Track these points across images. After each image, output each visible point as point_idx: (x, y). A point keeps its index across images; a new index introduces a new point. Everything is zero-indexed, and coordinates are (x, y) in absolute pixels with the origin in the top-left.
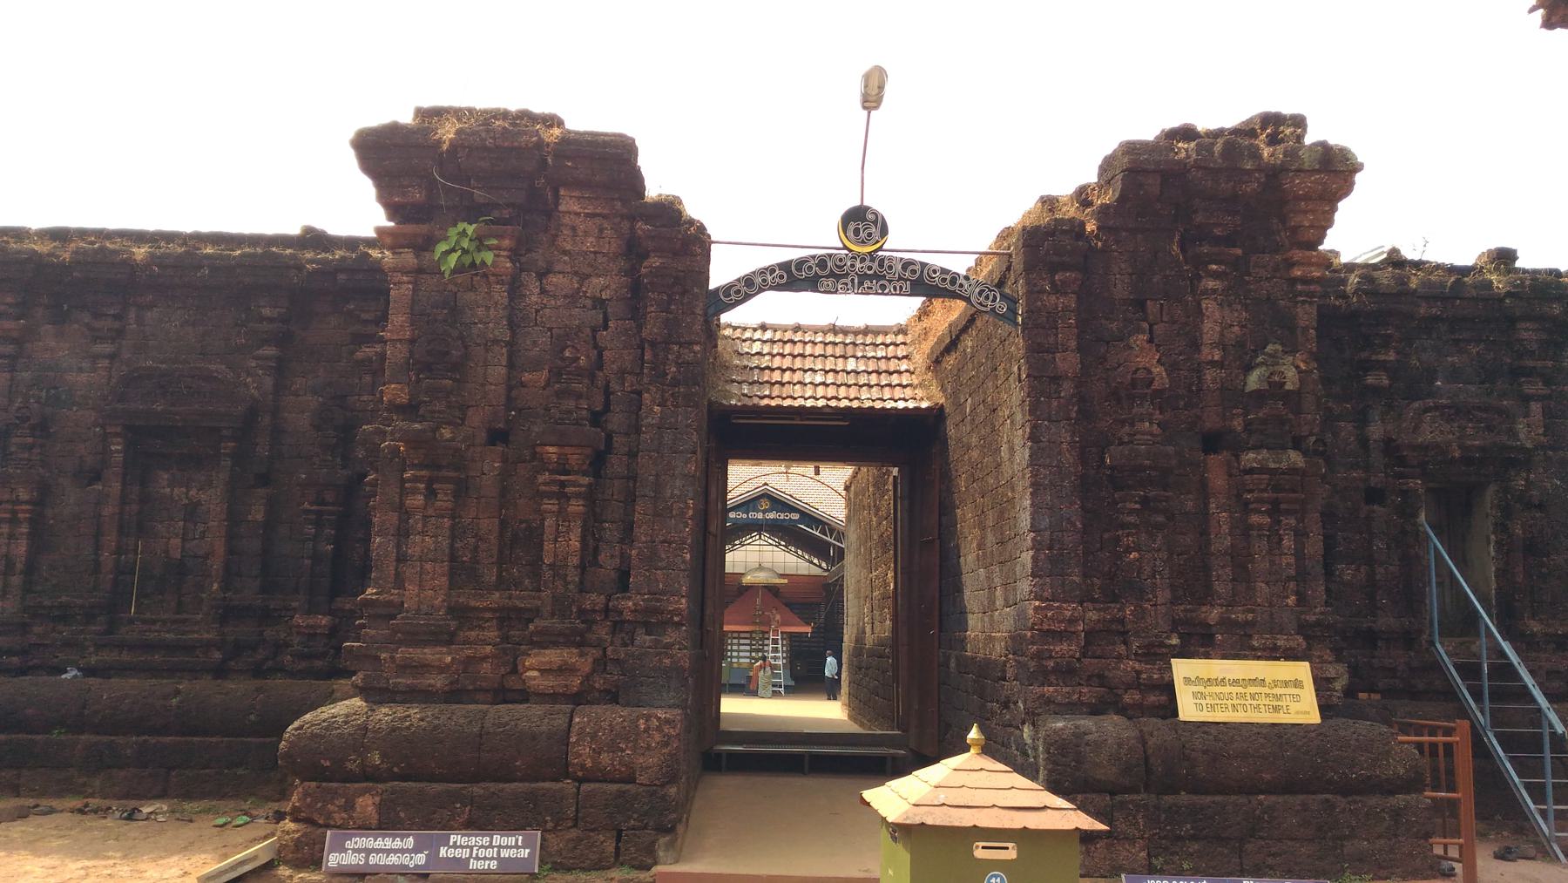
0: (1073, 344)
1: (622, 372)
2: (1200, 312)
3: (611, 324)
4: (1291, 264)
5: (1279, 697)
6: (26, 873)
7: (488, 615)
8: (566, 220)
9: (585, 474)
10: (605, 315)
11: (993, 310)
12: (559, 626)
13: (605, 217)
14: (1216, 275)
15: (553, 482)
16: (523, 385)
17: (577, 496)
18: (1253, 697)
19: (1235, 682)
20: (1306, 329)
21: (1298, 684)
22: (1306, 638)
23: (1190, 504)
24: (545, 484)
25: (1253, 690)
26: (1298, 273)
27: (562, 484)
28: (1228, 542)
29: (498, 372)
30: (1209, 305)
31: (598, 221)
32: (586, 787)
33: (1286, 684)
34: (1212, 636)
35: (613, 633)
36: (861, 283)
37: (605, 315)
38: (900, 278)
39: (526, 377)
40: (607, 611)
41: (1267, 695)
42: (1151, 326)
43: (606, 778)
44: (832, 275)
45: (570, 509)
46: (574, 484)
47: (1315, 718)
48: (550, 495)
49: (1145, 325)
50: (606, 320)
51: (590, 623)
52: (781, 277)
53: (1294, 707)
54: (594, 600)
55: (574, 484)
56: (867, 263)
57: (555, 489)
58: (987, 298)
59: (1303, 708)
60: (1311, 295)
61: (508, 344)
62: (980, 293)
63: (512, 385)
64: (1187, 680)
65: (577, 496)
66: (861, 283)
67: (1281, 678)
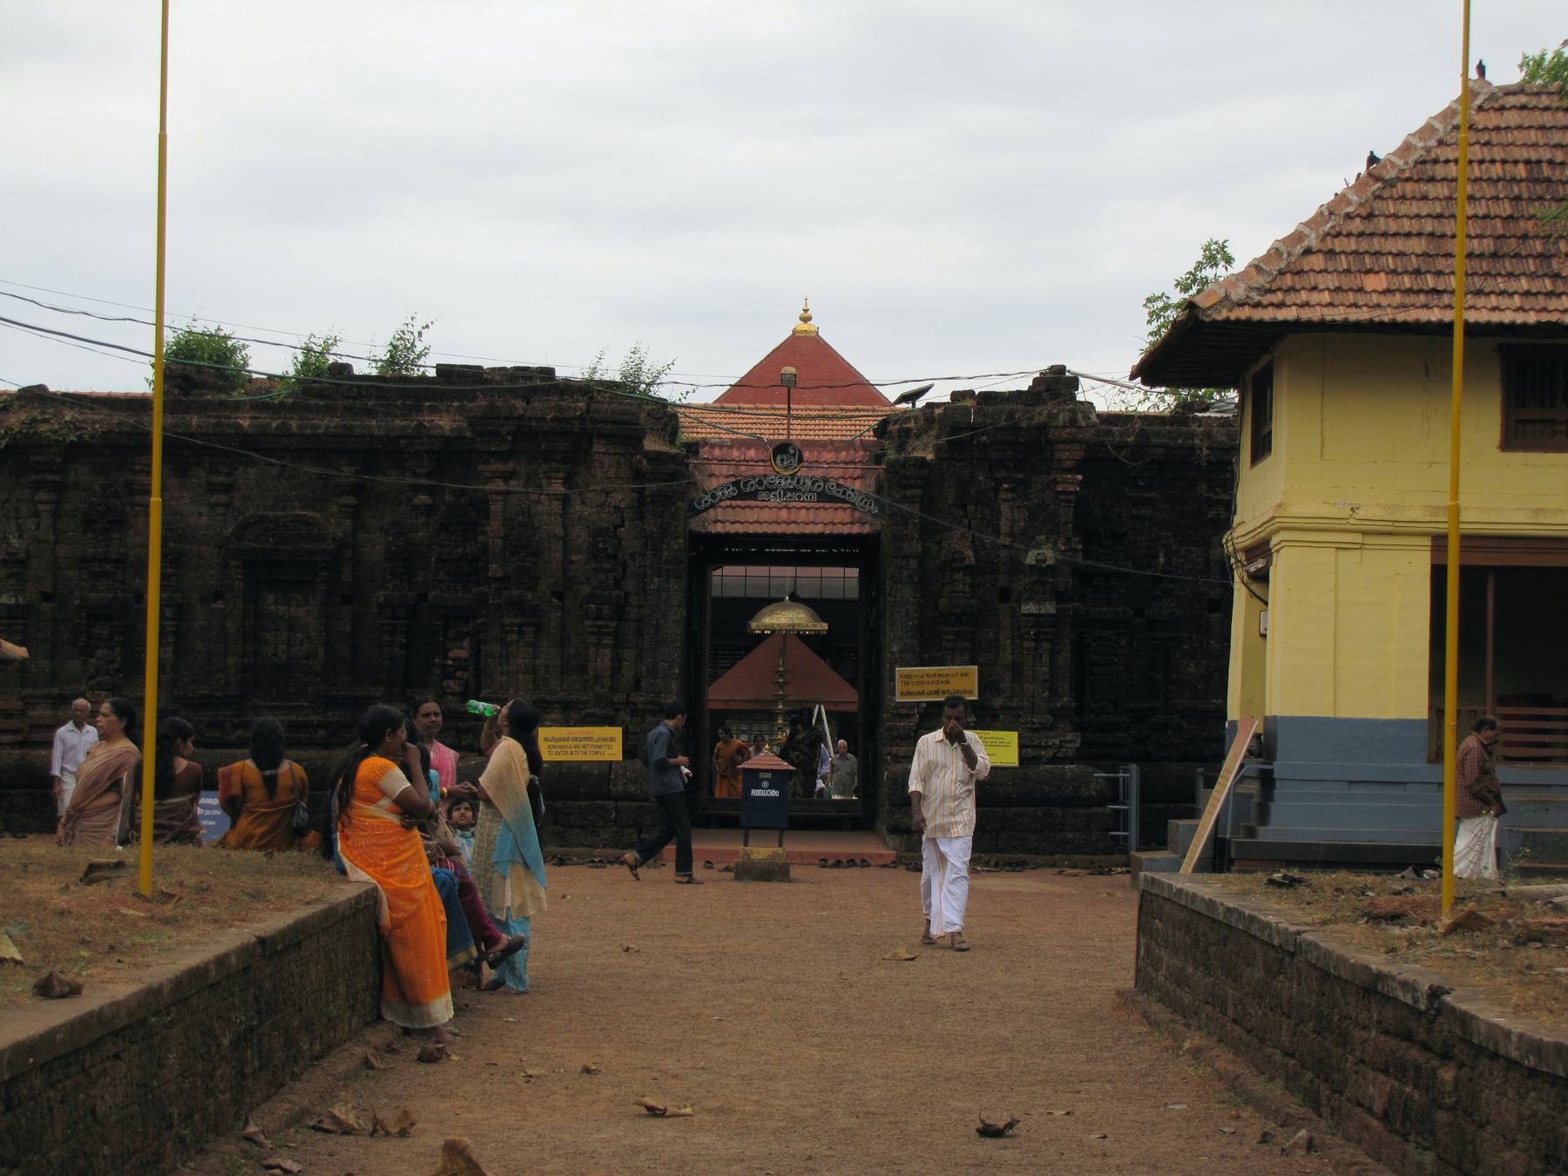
0: (917, 536)
1: (633, 555)
2: (999, 513)
3: (626, 523)
4: (1055, 482)
5: (600, 747)
6: (948, 989)
7: (557, 705)
8: (597, 457)
9: (612, 620)
10: (622, 517)
11: (870, 511)
12: (600, 712)
13: (622, 454)
14: (1007, 490)
15: (594, 626)
16: (572, 562)
17: (609, 634)
18: (584, 747)
19: (575, 739)
20: (1066, 523)
21: (612, 739)
22: (1053, 716)
23: (991, 634)
24: (590, 627)
25: (584, 743)
26: (1059, 488)
27: (599, 627)
28: (1010, 658)
29: (558, 555)
30: (1004, 508)
31: (617, 457)
32: (619, 803)
33: (605, 740)
34: (998, 716)
35: (632, 716)
36: (785, 495)
37: (622, 517)
38: (811, 491)
39: (574, 558)
40: (627, 703)
41: (592, 746)
42: (970, 521)
43: (633, 798)
44: (766, 489)
45: (604, 642)
46: (607, 626)
47: (619, 757)
48: (592, 633)
49: (966, 521)
50: (623, 521)
51: (617, 710)
52: (734, 491)
53: (607, 751)
54: (619, 697)
55: (607, 626)
56: (789, 481)
57: (595, 630)
58: (866, 503)
59: (615, 752)
60: (1069, 501)
61: (563, 538)
62: (862, 500)
63: (566, 561)
64: (546, 739)
65: (609, 634)
66: (785, 495)
67: (604, 736)
